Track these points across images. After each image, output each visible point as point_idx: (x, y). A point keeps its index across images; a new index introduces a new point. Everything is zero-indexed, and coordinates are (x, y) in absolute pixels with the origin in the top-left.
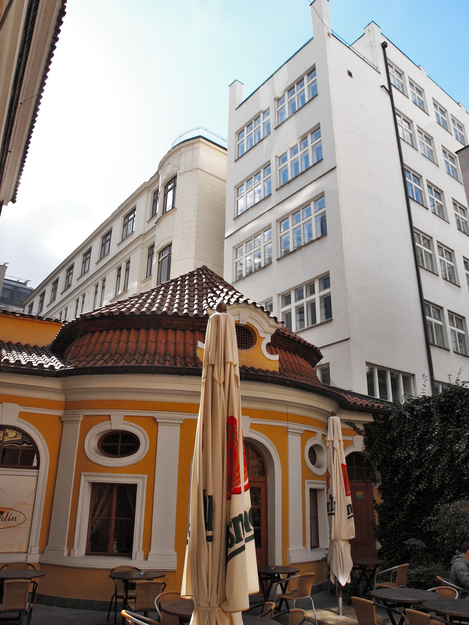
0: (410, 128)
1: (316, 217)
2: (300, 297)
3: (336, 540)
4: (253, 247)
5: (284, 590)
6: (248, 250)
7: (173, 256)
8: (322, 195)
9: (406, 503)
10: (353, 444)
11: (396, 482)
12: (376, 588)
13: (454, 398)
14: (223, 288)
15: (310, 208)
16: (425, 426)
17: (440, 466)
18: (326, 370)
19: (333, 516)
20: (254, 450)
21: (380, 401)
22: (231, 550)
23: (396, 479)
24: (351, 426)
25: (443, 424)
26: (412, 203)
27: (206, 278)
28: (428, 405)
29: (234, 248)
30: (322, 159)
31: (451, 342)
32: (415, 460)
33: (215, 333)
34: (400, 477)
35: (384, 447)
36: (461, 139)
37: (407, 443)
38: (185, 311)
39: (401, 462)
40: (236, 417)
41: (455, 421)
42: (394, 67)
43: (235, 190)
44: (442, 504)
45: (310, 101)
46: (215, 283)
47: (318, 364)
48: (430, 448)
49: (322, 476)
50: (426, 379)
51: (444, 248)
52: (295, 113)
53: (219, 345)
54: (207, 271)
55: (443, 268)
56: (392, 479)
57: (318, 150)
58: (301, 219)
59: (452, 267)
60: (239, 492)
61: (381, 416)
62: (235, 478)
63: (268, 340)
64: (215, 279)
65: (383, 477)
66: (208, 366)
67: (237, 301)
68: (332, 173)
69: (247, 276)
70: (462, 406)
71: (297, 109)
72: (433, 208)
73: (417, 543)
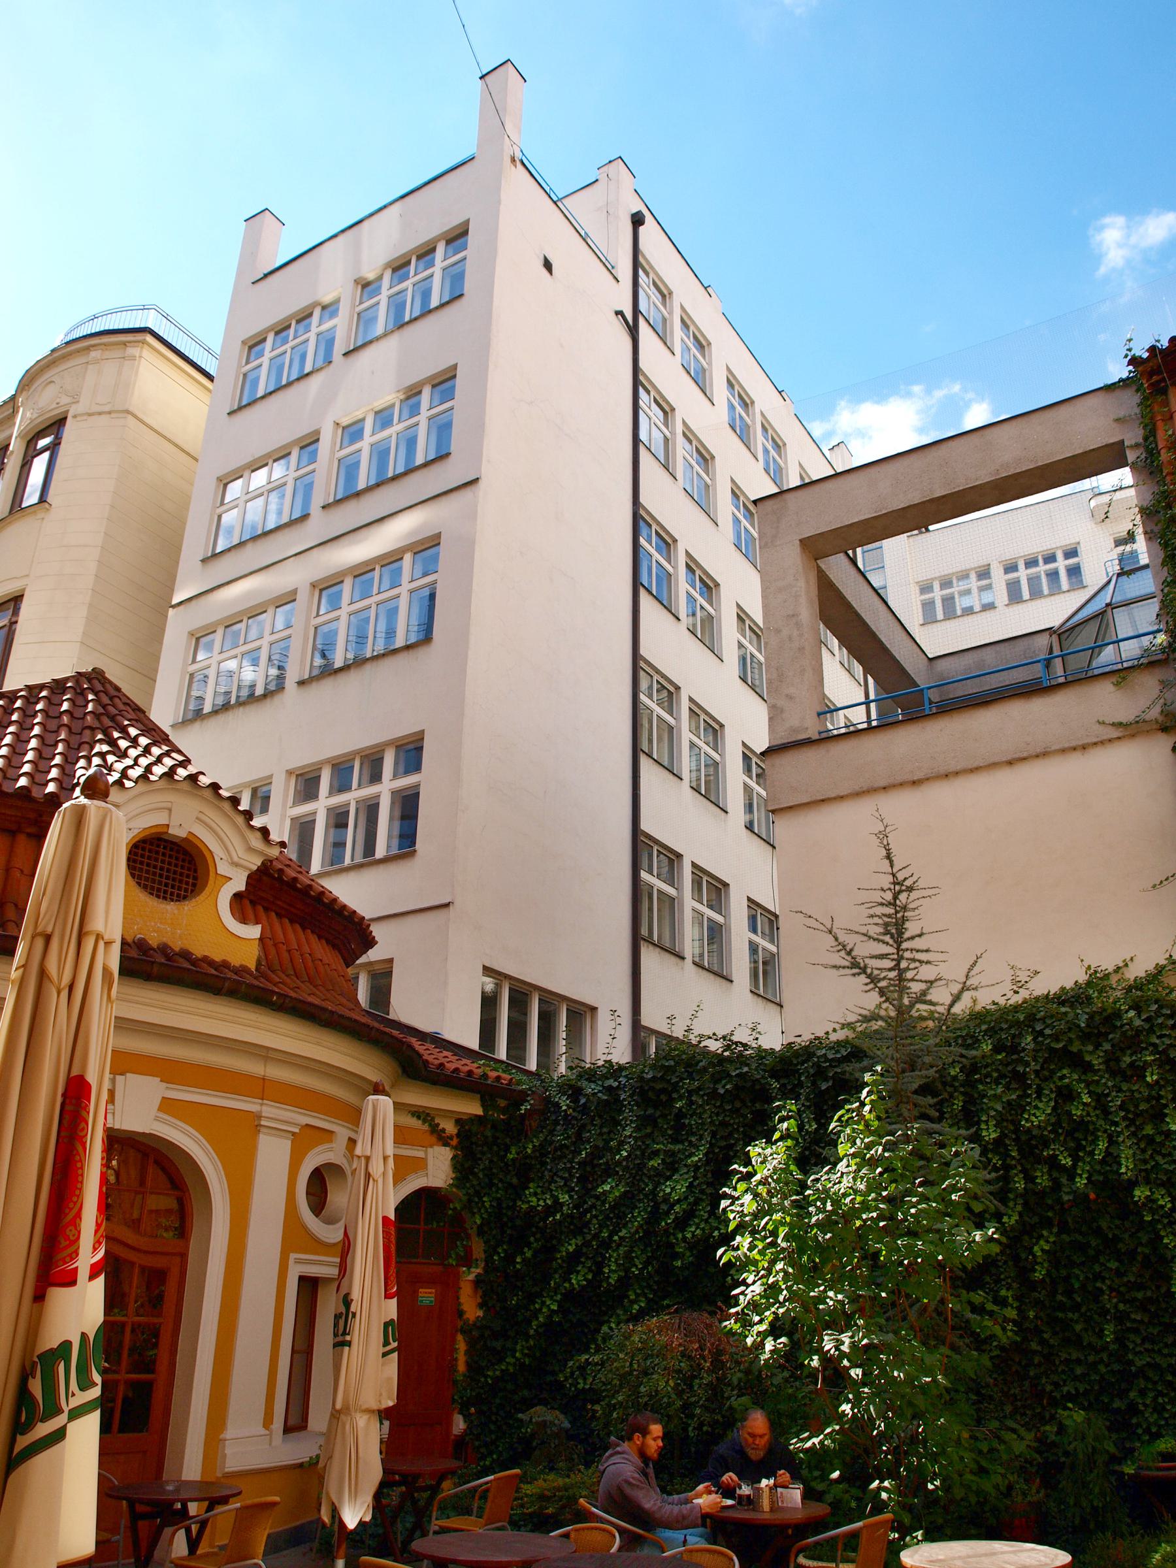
0: (666, 425)
1: (411, 592)
2: (341, 786)
3: (346, 1410)
4: (242, 642)
5: (193, 1544)
6: (227, 645)
7: (20, 628)
8: (434, 541)
9: (537, 1319)
10: (425, 1167)
11: (518, 1266)
12: (435, 1533)
13: (674, 1072)
14: (137, 736)
15: (401, 568)
16: (601, 1134)
17: (624, 1231)
18: (382, 977)
19: (347, 1348)
20: (163, 1169)
21: (503, 1066)
22: (23, 1441)
23: (518, 1260)
24: (424, 1121)
25: (643, 1133)
26: (645, 600)
27: (97, 701)
28: (615, 1084)
29: (191, 634)
30: (448, 455)
31: (690, 939)
32: (568, 1216)
33: (69, 849)
34: (529, 1254)
35: (501, 1180)
36: (775, 472)
37: (555, 1174)
38: (23, 782)
39: (537, 1219)
40: (92, 1078)
41: (671, 1128)
42: (652, 275)
43: (218, 487)
44: (618, 1324)
45: (442, 306)
46: (119, 718)
47: (362, 960)
48: (607, 1187)
49: (334, 1245)
50: (618, 1020)
51: (703, 716)
52: (401, 326)
53: (72, 887)
54: (103, 685)
55: (694, 764)
56: (509, 1259)
57: (443, 429)
58: (375, 591)
59: (716, 764)
60: (70, 1280)
61: (502, 1103)
62: (64, 1243)
63: (239, 883)
64: (121, 707)
65: (490, 1252)
66: (33, 938)
67: (170, 774)
68: (467, 494)
69: (215, 712)
70: (690, 1092)
71: (407, 318)
72: (691, 618)
73: (549, 1418)
